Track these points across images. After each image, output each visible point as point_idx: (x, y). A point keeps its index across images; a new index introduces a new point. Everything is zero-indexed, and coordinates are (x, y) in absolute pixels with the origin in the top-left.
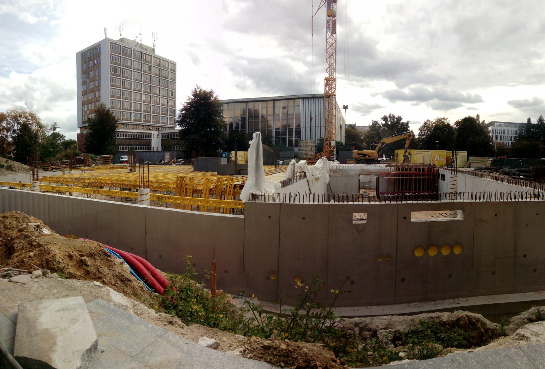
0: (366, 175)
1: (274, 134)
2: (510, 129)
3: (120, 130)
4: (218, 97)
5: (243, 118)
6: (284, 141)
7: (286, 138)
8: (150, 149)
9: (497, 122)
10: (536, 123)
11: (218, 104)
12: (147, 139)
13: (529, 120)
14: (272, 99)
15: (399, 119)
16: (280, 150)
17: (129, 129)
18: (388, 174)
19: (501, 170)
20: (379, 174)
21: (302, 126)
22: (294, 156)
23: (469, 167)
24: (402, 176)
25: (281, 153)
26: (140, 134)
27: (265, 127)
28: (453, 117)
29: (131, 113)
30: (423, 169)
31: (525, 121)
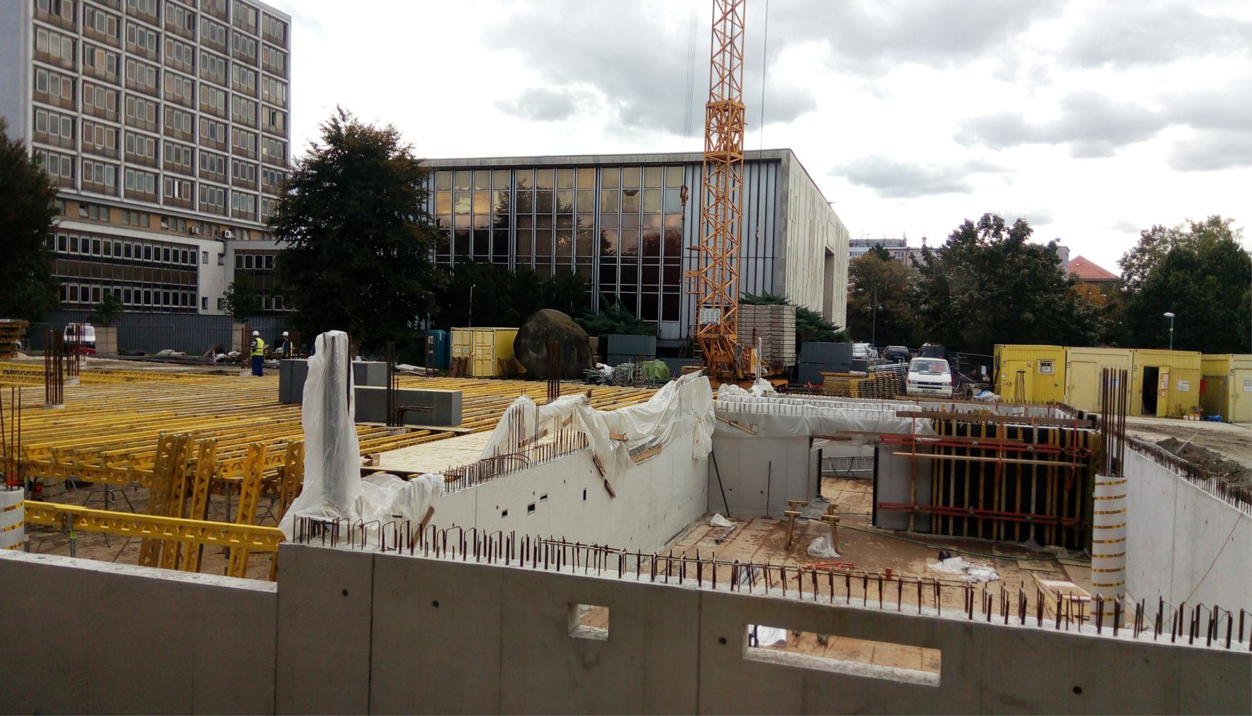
3: (65, 225)
4: (413, 152)
5: (504, 220)
6: (629, 301)
7: (635, 289)
8: (193, 302)
11: (414, 173)
12: (183, 270)
14: (590, 161)
15: (1022, 229)
16: (612, 330)
17: (108, 223)
18: (908, 442)
20: (877, 438)
21: (687, 244)
22: (653, 352)
24: (961, 451)
25: (614, 341)
26: (143, 246)
29: (117, 168)
30: (1044, 434)
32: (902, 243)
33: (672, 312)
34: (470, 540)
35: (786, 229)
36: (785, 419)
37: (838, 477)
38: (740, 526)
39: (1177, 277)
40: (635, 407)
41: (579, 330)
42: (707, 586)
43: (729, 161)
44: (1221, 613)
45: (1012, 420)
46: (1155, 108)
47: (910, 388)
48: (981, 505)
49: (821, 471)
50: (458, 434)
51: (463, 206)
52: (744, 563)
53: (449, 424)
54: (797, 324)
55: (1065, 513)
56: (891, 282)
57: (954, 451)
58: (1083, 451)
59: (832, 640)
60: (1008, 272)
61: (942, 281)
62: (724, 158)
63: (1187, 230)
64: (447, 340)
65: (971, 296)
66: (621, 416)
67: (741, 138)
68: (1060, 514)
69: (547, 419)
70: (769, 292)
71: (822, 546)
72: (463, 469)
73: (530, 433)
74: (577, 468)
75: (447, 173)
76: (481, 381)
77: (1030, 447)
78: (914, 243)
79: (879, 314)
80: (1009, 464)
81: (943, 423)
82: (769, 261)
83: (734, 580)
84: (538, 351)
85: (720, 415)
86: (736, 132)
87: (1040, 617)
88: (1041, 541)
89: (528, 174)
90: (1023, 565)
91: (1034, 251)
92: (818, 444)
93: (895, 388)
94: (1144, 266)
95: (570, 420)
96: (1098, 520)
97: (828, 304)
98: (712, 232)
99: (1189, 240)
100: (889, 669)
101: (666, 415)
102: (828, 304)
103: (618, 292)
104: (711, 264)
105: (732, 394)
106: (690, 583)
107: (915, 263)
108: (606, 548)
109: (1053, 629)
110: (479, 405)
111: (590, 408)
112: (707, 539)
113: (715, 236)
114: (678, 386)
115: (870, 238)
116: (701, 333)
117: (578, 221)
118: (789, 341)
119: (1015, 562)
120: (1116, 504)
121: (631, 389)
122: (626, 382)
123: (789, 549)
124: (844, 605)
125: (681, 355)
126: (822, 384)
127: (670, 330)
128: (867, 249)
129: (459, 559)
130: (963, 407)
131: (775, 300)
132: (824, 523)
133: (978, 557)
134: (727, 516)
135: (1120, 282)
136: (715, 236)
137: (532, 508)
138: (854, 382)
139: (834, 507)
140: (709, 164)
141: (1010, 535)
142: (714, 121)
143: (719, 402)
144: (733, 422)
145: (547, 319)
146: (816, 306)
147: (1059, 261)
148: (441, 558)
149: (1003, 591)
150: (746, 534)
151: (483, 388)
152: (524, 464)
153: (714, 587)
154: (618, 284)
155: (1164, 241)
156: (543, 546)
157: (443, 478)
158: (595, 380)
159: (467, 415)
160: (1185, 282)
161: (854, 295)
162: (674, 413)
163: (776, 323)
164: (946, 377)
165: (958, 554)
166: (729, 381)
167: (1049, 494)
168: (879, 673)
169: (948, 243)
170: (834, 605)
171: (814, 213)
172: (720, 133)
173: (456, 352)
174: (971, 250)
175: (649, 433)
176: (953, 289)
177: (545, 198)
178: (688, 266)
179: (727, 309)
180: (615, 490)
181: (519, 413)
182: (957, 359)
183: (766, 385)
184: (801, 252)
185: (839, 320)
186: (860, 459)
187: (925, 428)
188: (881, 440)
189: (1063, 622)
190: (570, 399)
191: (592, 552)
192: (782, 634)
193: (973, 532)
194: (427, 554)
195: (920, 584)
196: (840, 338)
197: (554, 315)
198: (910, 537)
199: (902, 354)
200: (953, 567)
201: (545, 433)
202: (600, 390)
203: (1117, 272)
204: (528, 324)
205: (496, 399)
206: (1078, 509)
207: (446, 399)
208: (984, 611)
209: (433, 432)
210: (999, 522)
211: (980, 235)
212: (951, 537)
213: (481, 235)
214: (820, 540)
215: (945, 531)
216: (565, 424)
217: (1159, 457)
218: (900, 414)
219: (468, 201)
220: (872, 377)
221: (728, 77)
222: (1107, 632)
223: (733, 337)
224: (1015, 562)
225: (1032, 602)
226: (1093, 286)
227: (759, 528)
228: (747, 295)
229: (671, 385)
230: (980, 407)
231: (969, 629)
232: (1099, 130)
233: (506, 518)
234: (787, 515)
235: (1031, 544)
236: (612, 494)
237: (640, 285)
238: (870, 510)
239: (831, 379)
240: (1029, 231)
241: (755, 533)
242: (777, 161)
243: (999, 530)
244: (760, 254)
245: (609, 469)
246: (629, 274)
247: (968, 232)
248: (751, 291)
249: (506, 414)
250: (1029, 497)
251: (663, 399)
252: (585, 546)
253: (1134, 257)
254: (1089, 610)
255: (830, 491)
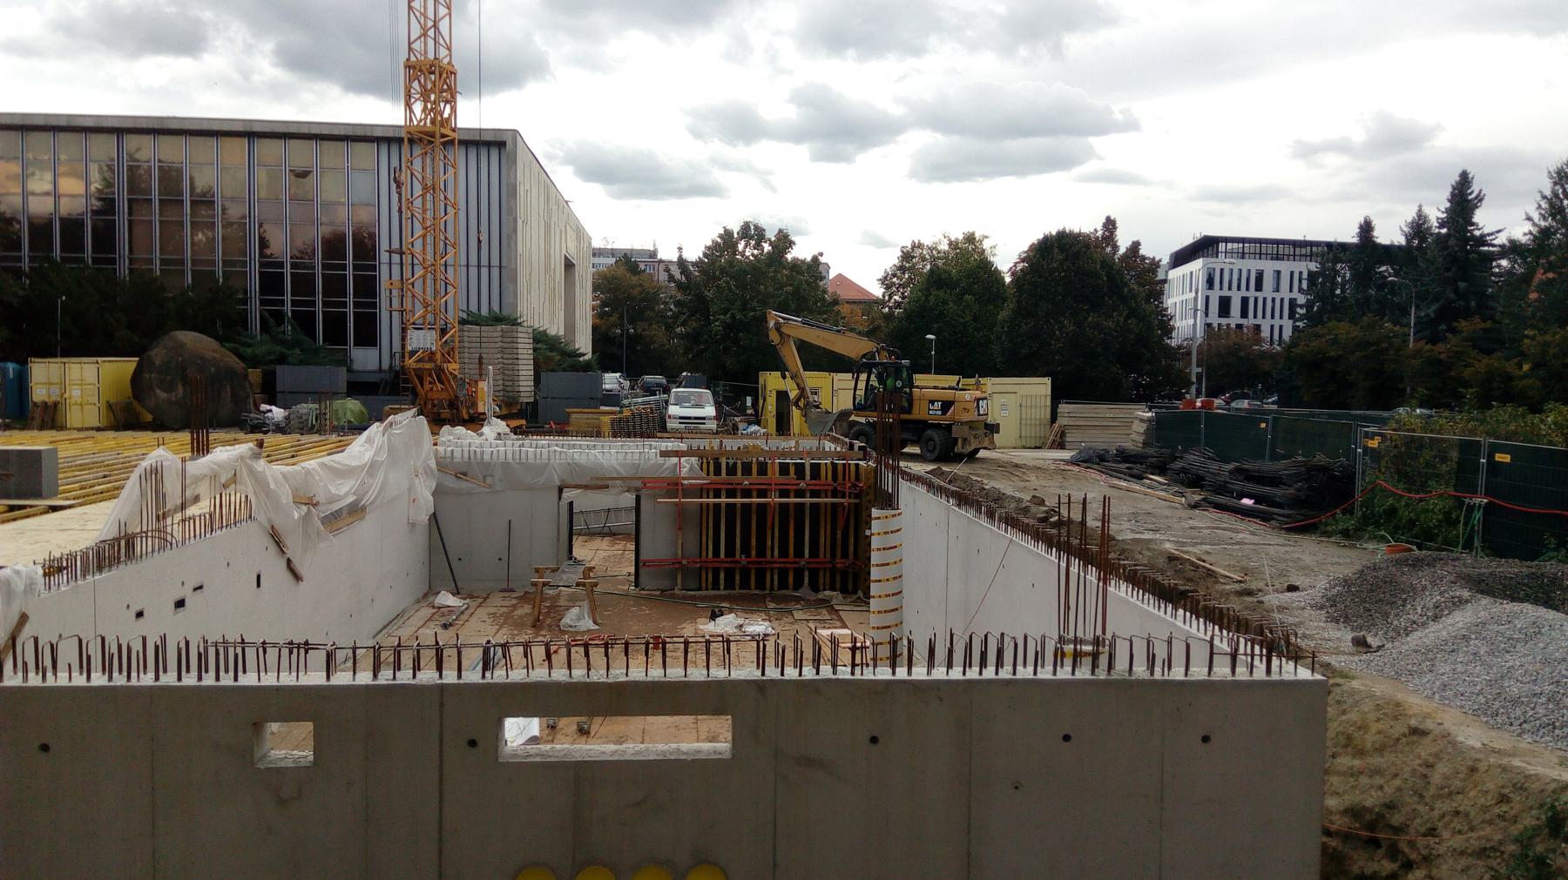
0: (586, 487)
1: (255, 284)
2: (1285, 267)
5: (108, 205)
6: (305, 321)
7: (313, 304)
9: (1227, 240)
10: (1401, 240)
13: (1366, 228)
14: (240, 128)
15: (784, 242)
16: (282, 360)
18: (674, 486)
19: (1178, 465)
20: (638, 484)
21: (384, 245)
22: (343, 387)
23: (1061, 446)
24: (731, 493)
25: (286, 376)
27: (213, 250)
28: (1009, 225)
30: (816, 469)
31: (1348, 234)
32: (653, 254)
33: (368, 336)
34: (95, 651)
35: (515, 231)
36: (525, 466)
37: (592, 534)
38: (474, 604)
39: (937, 296)
40: (327, 460)
41: (233, 361)
42: (450, 677)
43: (438, 140)
44: (1007, 639)
45: (784, 454)
46: (897, 111)
47: (671, 425)
48: (754, 553)
49: (572, 527)
50: (54, 509)
51: (41, 183)
52: (476, 645)
53: (38, 495)
54: (535, 350)
55: (839, 552)
56: (643, 300)
57: (723, 493)
58: (855, 486)
59: (597, 724)
60: (771, 289)
61: (701, 298)
62: (432, 135)
63: (944, 247)
64: (22, 381)
65: (733, 316)
66: (308, 472)
67: (454, 110)
68: (833, 556)
69: (198, 479)
70: (496, 308)
71: (578, 619)
72: (72, 557)
73: (173, 499)
74: (249, 544)
75: (12, 134)
76: (83, 434)
77: (802, 485)
78: (668, 254)
79: (630, 337)
80: (781, 504)
81: (712, 462)
82: (495, 271)
83: (487, 665)
84: (169, 388)
85: (444, 465)
86: (447, 102)
87: (834, 666)
88: (815, 587)
89: (147, 140)
90: (798, 615)
91: (797, 265)
92: (568, 495)
93: (652, 425)
94: (903, 286)
95: (234, 479)
96: (875, 558)
97: (570, 326)
98: (419, 232)
99: (946, 258)
100: (674, 746)
101: (373, 467)
102: (570, 326)
103: (288, 309)
104: (419, 272)
105: (457, 439)
106: (428, 676)
107: (671, 278)
108: (306, 643)
109: (849, 677)
110: (82, 467)
111: (262, 462)
112: (431, 624)
113: (424, 236)
114: (385, 430)
115: (616, 246)
116: (410, 363)
117: (224, 210)
118: (526, 371)
119: (790, 613)
120: (892, 540)
121: (316, 437)
122: (306, 428)
123: (537, 624)
124: (623, 679)
125: (386, 391)
126: (567, 423)
127: (365, 359)
128: (612, 261)
129: (79, 680)
130: (731, 444)
131: (504, 320)
132: (580, 590)
133: (752, 612)
134: (456, 592)
135: (877, 302)
136: (424, 236)
137: (180, 604)
138: (606, 419)
139: (591, 569)
140: (411, 141)
141: (783, 585)
142: (416, 84)
143: (440, 449)
144: (461, 474)
145: (182, 346)
146: (556, 329)
147: (822, 278)
148: (51, 681)
149: (796, 640)
150: (482, 613)
151: (88, 444)
152: (164, 542)
153: (460, 677)
154: (288, 297)
155: (923, 259)
156: (212, 651)
157: (40, 571)
158: (259, 427)
159: (67, 481)
160: (945, 303)
161: (600, 314)
162: (383, 461)
163: (510, 348)
164: (710, 411)
165: (731, 611)
166: (453, 423)
167: (822, 533)
168: (664, 752)
169: (705, 255)
170: (611, 680)
171: (549, 211)
172: (425, 102)
173: (39, 393)
174: (731, 263)
175: (347, 494)
176: (714, 308)
177: (171, 177)
178: (387, 275)
179: (443, 332)
180: (302, 570)
181: (156, 473)
182: (720, 389)
183: (502, 426)
184: (535, 265)
185: (584, 343)
186: (618, 510)
187: (691, 469)
188: (642, 486)
189: (858, 670)
190: (228, 452)
191: (285, 652)
192: (533, 726)
193: (745, 584)
194: (25, 678)
195: (708, 642)
196: (587, 367)
197: (189, 339)
198: (678, 597)
199: (659, 385)
200: (726, 624)
201: (196, 499)
202: (271, 439)
203: (877, 291)
204: (153, 353)
205: (109, 458)
206: (851, 548)
207: (33, 458)
208: (777, 666)
209: (12, 508)
210: (772, 570)
211: (741, 247)
212: (723, 592)
213: (72, 226)
214: (575, 611)
215: (716, 586)
216: (225, 486)
217: (930, 486)
218: (665, 454)
219: (49, 176)
220: (626, 413)
221: (431, 29)
222: (902, 673)
223: (453, 367)
224: (790, 613)
225: (826, 651)
226: (855, 307)
227: (498, 603)
228: (469, 313)
229: (376, 429)
230: (750, 442)
231: (761, 686)
232: (839, 132)
233: (141, 620)
234: (534, 584)
235: (805, 591)
236: (297, 577)
237: (319, 298)
238: (632, 570)
239: (578, 417)
240: (791, 244)
241: (493, 610)
242: (501, 145)
243: (773, 579)
244: (484, 261)
245: (291, 543)
246: (303, 283)
247: (727, 241)
248: (474, 308)
249: (134, 477)
250: (796, 545)
251: (363, 448)
252: (274, 645)
253: (894, 275)
254: (884, 651)
255: (581, 550)
